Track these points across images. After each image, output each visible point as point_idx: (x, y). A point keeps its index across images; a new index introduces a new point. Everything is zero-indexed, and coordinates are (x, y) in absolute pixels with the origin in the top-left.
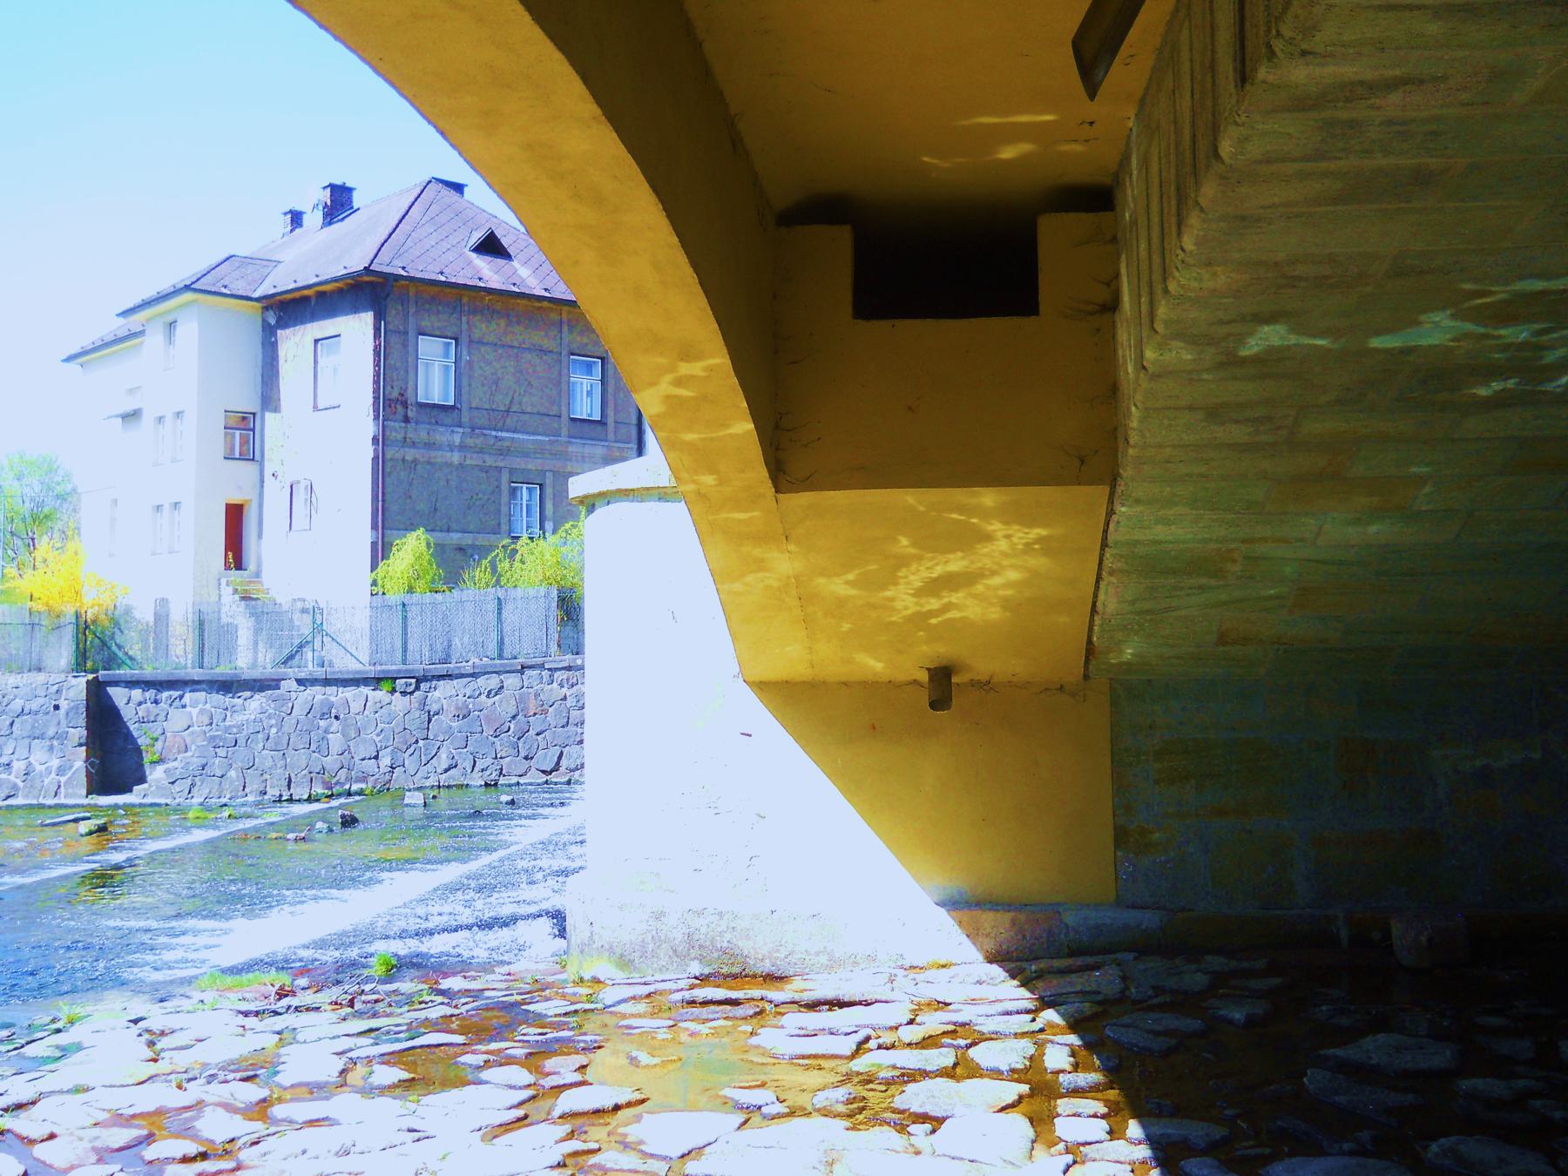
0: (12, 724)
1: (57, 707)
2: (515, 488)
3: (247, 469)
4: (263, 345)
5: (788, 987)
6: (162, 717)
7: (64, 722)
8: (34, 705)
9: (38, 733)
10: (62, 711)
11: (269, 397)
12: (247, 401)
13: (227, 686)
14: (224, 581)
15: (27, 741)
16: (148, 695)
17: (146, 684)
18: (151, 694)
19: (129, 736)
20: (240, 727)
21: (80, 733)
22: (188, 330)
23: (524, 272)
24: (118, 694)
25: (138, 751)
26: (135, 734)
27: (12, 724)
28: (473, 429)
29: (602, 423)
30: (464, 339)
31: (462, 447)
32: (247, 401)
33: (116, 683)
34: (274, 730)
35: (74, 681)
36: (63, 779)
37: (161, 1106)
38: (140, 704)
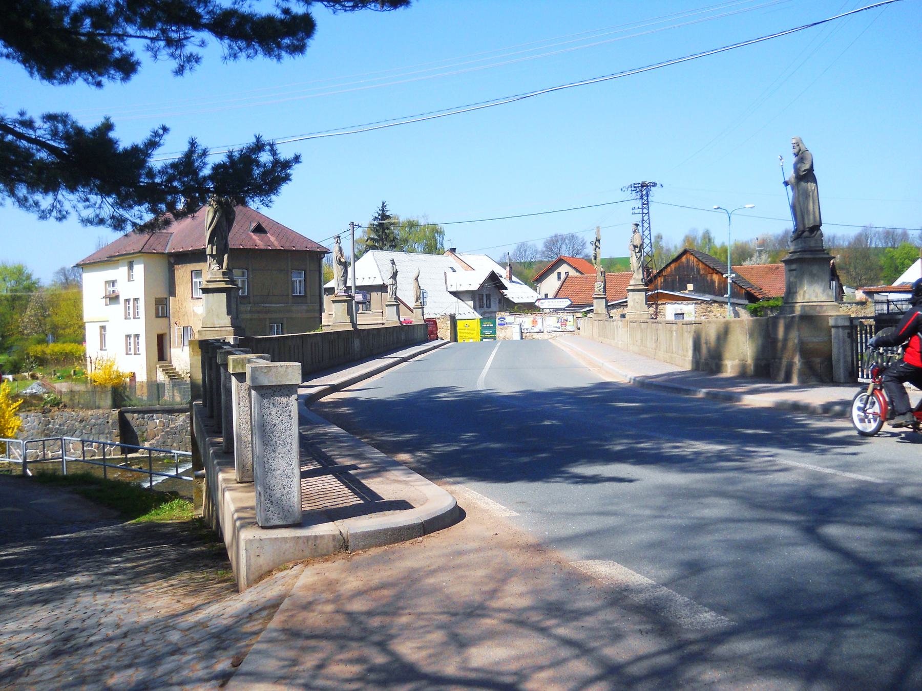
0: (91, 429)
1: (108, 422)
2: (272, 326)
3: (164, 321)
4: (169, 270)
5: (753, 460)
6: (146, 424)
7: (111, 428)
8: (99, 422)
9: (102, 432)
10: (110, 424)
11: (172, 292)
12: (162, 294)
13: (170, 411)
14: (158, 366)
15: (98, 435)
16: (140, 416)
17: (139, 412)
18: (140, 416)
19: (133, 431)
20: (176, 427)
21: (116, 431)
22: (139, 269)
23: (272, 239)
24: (129, 416)
25: (136, 436)
26: (136, 431)
27: (91, 429)
28: (254, 304)
29: (305, 296)
30: (250, 269)
31: (251, 312)
32: (162, 294)
33: (128, 412)
34: (189, 428)
35: (114, 412)
36: (112, 449)
37: (809, 403)
38: (137, 419)
